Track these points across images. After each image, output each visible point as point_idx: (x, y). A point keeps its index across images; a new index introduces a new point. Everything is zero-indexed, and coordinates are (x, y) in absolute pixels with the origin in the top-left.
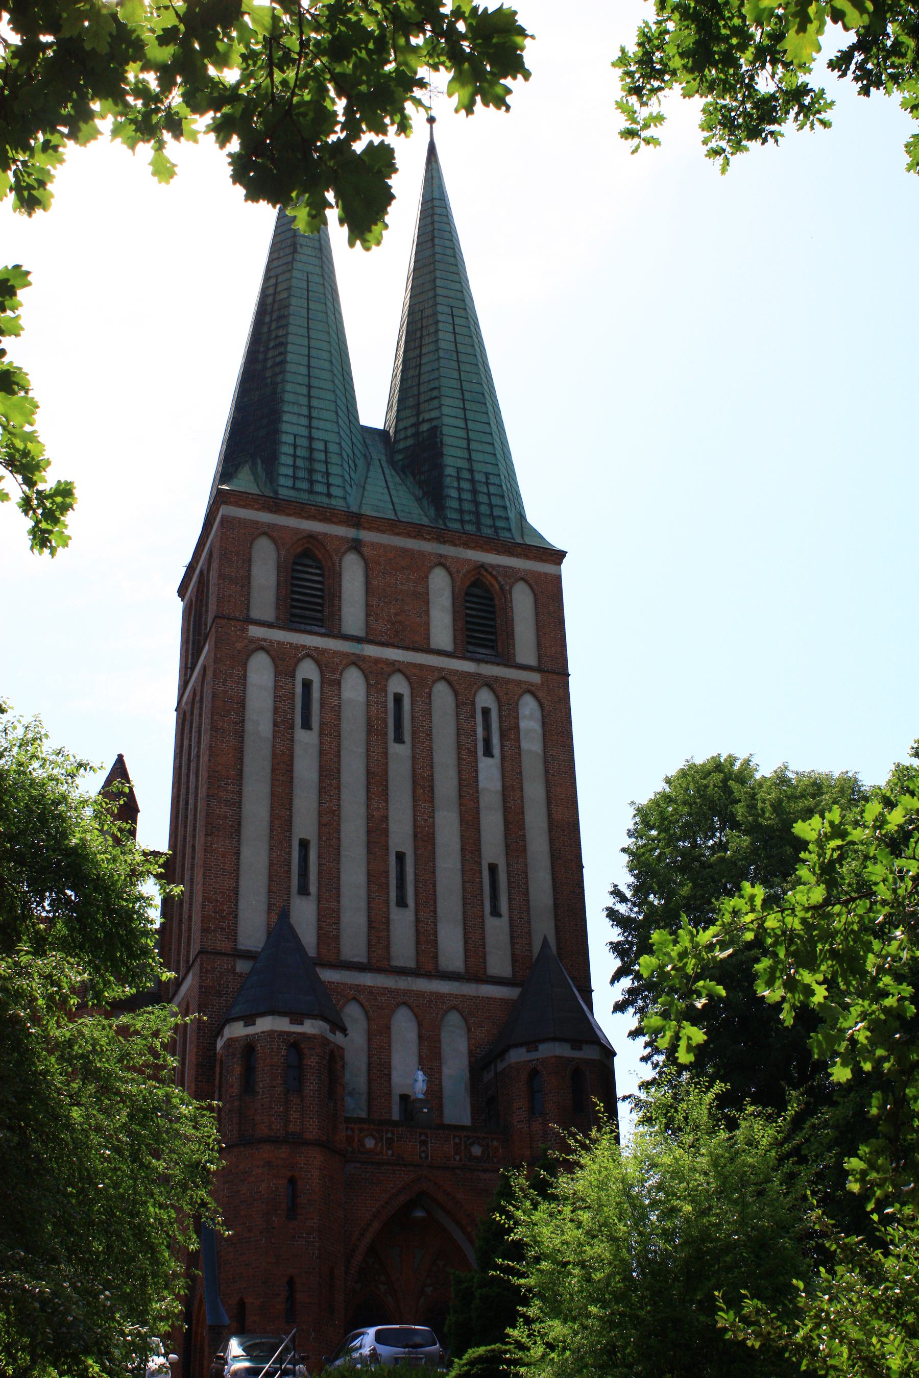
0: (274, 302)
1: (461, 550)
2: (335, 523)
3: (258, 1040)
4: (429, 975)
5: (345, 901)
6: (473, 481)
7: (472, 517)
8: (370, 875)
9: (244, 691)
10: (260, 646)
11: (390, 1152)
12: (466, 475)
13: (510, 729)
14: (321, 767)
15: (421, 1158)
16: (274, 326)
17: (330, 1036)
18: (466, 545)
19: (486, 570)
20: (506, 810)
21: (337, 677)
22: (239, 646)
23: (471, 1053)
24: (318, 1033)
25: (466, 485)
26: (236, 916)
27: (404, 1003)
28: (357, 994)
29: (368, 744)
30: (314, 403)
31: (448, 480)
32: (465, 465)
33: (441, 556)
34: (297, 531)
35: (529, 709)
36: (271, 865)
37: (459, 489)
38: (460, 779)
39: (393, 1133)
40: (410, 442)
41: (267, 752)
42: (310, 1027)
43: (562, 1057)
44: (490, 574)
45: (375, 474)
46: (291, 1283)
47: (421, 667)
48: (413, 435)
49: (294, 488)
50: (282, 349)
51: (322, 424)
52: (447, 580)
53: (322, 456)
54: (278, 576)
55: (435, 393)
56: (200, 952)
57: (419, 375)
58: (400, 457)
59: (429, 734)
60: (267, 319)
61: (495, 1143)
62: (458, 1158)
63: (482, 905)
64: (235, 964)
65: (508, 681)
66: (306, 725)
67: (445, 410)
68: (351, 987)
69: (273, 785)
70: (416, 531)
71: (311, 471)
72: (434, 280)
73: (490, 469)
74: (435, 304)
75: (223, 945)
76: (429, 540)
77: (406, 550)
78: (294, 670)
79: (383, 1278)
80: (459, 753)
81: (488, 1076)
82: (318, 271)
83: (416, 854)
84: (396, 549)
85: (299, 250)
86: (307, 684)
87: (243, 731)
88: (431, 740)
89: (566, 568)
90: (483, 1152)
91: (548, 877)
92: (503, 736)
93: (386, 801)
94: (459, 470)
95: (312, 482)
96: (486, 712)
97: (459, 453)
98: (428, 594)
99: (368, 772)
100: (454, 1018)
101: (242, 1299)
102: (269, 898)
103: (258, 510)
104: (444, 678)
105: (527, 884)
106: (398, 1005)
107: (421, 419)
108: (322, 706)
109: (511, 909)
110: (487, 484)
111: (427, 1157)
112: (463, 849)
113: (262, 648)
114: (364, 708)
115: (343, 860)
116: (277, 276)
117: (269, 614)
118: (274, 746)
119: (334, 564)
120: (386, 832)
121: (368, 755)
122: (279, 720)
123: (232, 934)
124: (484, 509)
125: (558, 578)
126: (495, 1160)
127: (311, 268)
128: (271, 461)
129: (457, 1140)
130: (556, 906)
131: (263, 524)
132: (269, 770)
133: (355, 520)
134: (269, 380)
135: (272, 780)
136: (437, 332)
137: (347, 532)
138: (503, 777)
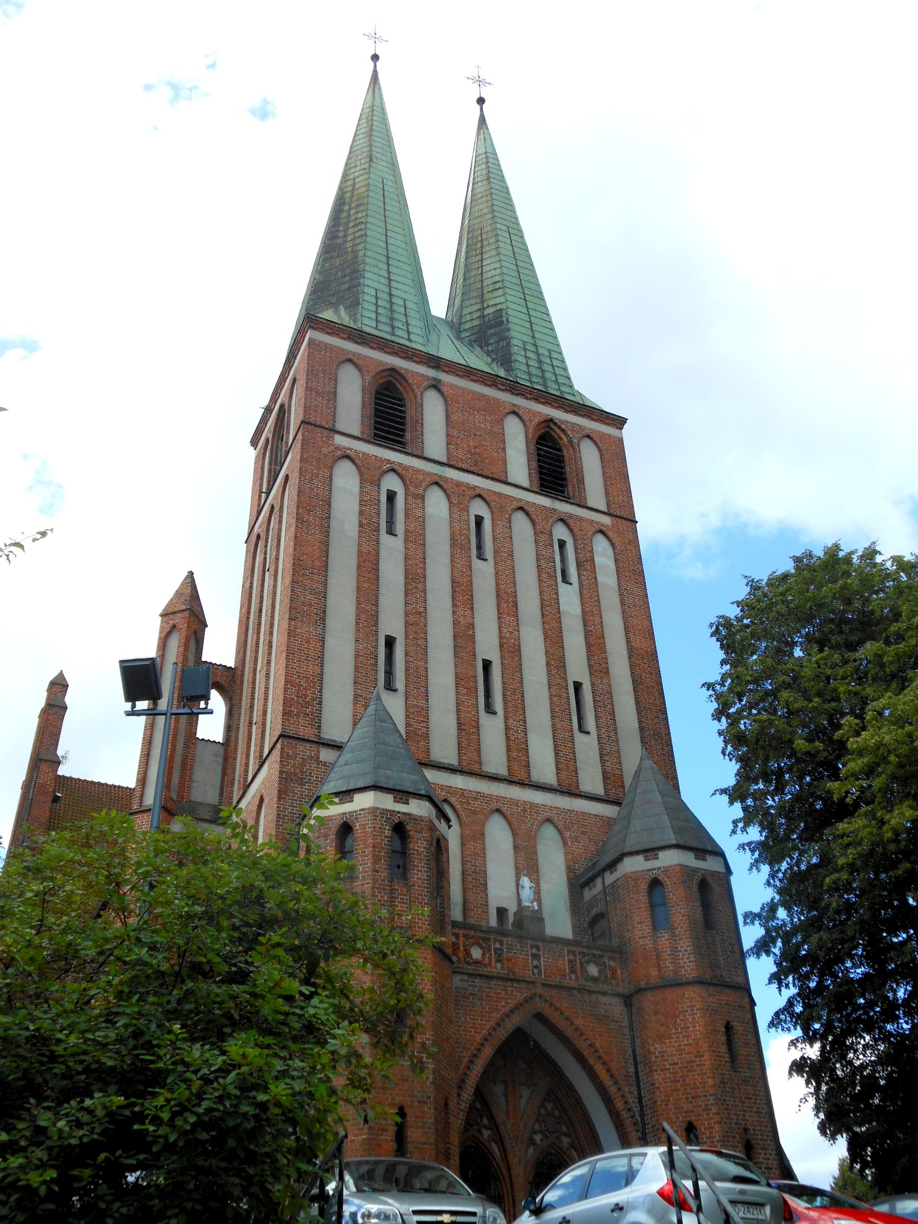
0: (352, 196)
3: (356, 819)
4: (521, 784)
8: (458, 679)
9: (330, 490)
12: (530, 347)
13: (586, 561)
15: (533, 973)
17: (436, 822)
19: (555, 424)
20: (587, 634)
21: (421, 492)
22: (325, 450)
23: (569, 869)
24: (426, 815)
26: (320, 703)
27: (498, 811)
29: (452, 556)
31: (515, 349)
32: (530, 340)
33: (514, 405)
34: (381, 363)
36: (357, 656)
37: (526, 357)
39: (502, 944)
41: (353, 550)
42: (418, 808)
43: (687, 866)
44: (559, 427)
47: (500, 495)
49: (376, 328)
50: (363, 226)
51: (400, 286)
56: (281, 736)
57: (482, 273)
59: (511, 555)
62: (573, 977)
63: (570, 719)
64: (318, 752)
65: (581, 519)
66: (391, 532)
69: (358, 581)
70: (492, 381)
73: (551, 347)
75: (307, 732)
76: (503, 390)
77: (483, 395)
78: (379, 480)
79: (485, 1121)
80: (540, 576)
81: (588, 894)
82: (392, 178)
83: (502, 664)
85: (374, 160)
88: (513, 560)
89: (627, 433)
90: (600, 972)
92: (579, 565)
93: (472, 609)
94: (524, 343)
95: (393, 327)
98: (504, 435)
99: (453, 581)
100: (549, 832)
102: (355, 690)
105: (612, 704)
107: (485, 305)
109: (598, 727)
110: (551, 358)
111: (540, 974)
112: (548, 664)
113: (348, 457)
114: (447, 523)
116: (354, 179)
118: (359, 545)
119: (415, 396)
120: (472, 638)
122: (365, 521)
123: (316, 721)
125: (621, 441)
128: (354, 306)
130: (641, 729)
131: (349, 352)
134: (350, 250)
135: (359, 575)
137: (431, 373)
138: (583, 603)
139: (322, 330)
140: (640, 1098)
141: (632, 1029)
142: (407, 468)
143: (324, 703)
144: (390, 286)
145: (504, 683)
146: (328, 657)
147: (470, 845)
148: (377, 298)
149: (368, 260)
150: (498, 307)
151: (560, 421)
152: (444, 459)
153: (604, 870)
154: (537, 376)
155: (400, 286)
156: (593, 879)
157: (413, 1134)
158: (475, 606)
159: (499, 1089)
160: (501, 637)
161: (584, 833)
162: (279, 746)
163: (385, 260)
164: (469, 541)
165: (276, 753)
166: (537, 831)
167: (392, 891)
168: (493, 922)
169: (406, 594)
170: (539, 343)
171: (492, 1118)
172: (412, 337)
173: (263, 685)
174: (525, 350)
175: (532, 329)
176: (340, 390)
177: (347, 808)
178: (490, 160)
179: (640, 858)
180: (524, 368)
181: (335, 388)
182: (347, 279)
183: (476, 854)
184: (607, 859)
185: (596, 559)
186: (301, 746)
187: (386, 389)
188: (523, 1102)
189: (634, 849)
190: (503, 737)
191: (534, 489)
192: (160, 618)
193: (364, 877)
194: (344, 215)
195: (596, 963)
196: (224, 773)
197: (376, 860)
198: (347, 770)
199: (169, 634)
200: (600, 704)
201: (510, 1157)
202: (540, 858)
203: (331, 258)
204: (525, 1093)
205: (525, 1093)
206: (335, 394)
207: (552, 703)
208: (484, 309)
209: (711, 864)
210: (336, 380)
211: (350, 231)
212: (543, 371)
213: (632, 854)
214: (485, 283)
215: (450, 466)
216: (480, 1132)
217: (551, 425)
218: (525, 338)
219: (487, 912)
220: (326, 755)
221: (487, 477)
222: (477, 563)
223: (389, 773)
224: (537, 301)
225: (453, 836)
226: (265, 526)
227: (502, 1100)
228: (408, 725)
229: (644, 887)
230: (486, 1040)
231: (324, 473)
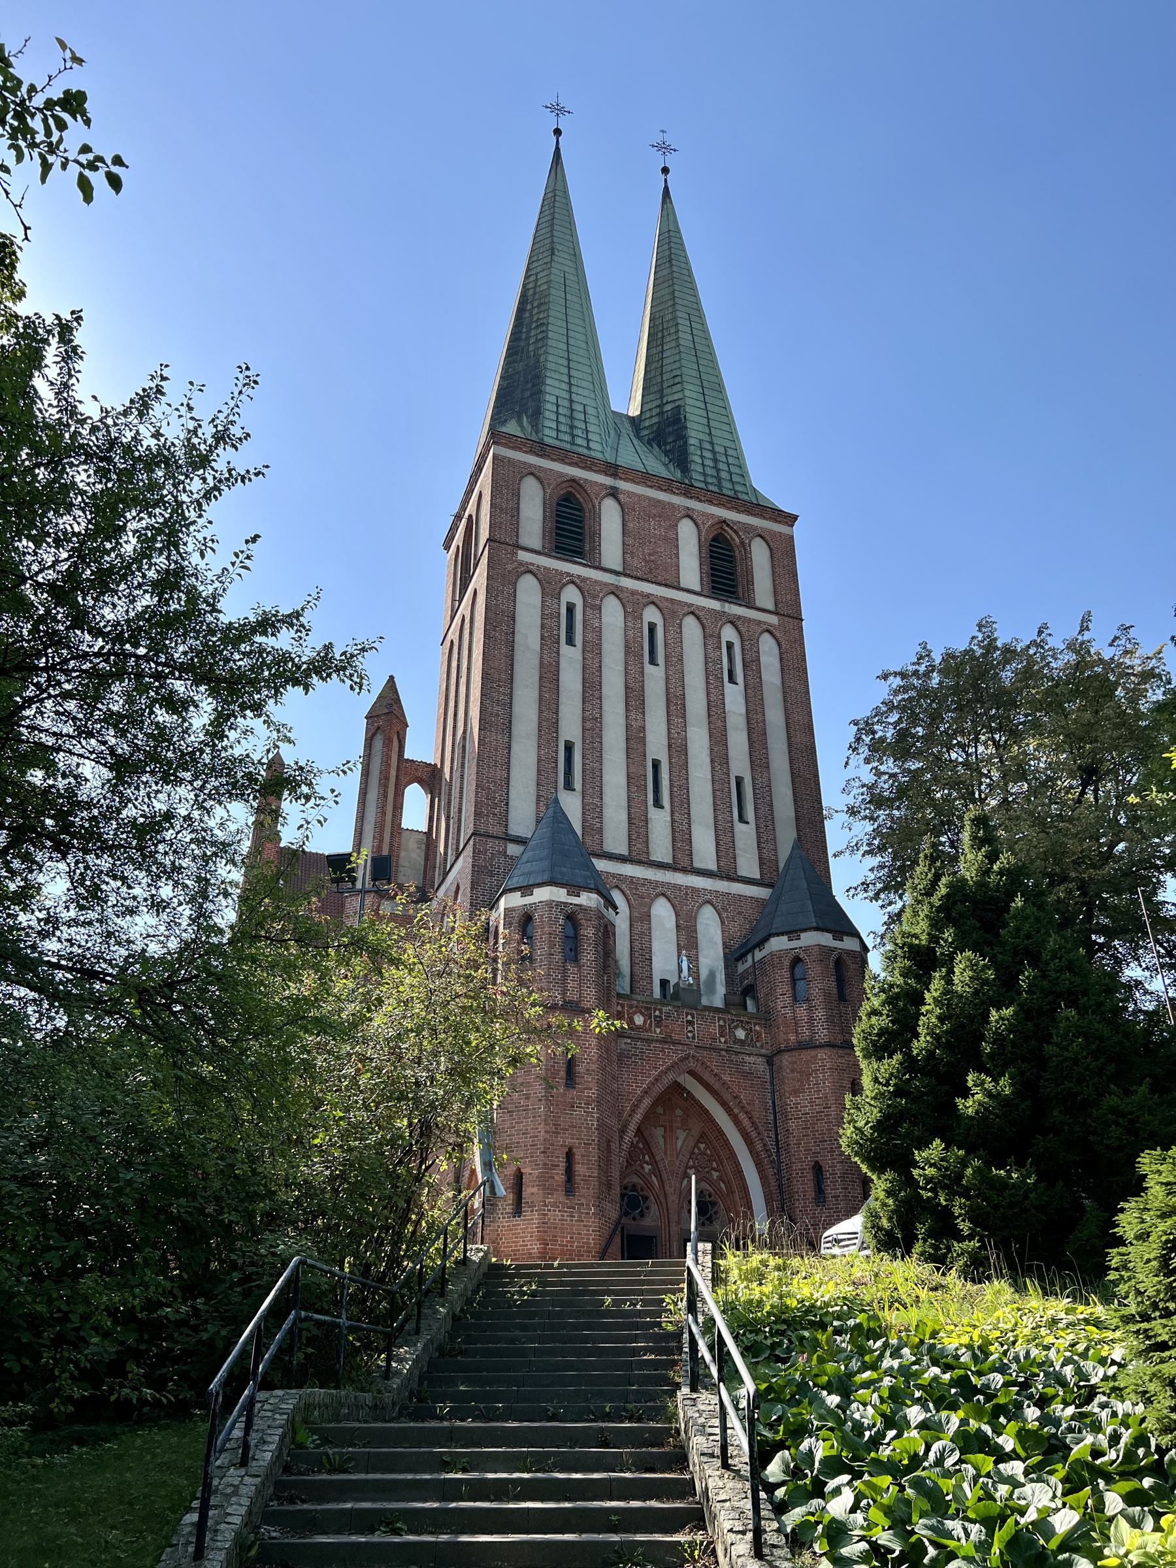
0: (535, 293)
1: (706, 505)
2: (595, 471)
4: (684, 870)
5: (607, 798)
6: (713, 452)
7: (714, 481)
11: (658, 1030)
14: (584, 679)
16: (535, 311)
17: (604, 911)
18: (711, 502)
19: (728, 525)
21: (598, 603)
22: (509, 567)
23: (725, 945)
25: (708, 455)
26: (507, 804)
27: (663, 895)
28: (621, 882)
30: (573, 373)
32: (707, 438)
34: (561, 475)
35: (768, 649)
36: (539, 761)
37: (702, 457)
38: (709, 702)
40: (655, 420)
42: (588, 899)
44: (732, 528)
45: (625, 441)
46: (569, 1155)
47: (672, 601)
48: (658, 414)
49: (557, 438)
50: (544, 328)
51: (580, 391)
52: (694, 530)
53: (582, 416)
54: (544, 511)
55: (678, 379)
56: (473, 834)
58: (646, 432)
60: (529, 307)
61: (757, 1028)
62: (723, 1040)
65: (749, 620)
66: (570, 642)
67: (687, 393)
68: (614, 876)
70: (666, 485)
71: (572, 427)
72: (673, 292)
73: (728, 443)
74: (675, 311)
75: (496, 830)
77: (659, 501)
79: (647, 1158)
80: (707, 678)
81: (742, 967)
82: (573, 271)
83: (670, 763)
84: (650, 499)
86: (571, 609)
87: (513, 641)
89: (798, 530)
91: (790, 793)
92: (745, 666)
93: (643, 713)
94: (701, 441)
95: (573, 436)
96: (730, 646)
97: (701, 428)
99: (627, 687)
101: (519, 1169)
103: (526, 452)
104: (692, 613)
105: (771, 796)
106: (657, 896)
108: (585, 627)
110: (726, 455)
111: (693, 1037)
115: (605, 762)
116: (537, 274)
117: (537, 544)
119: (594, 506)
120: (643, 740)
121: (626, 673)
123: (504, 820)
124: (724, 475)
125: (791, 538)
126: (758, 1044)
127: (567, 269)
128: (536, 416)
129: (722, 1023)
131: (531, 465)
132: (537, 679)
133: (612, 470)
136: (677, 331)
137: (607, 481)
139: (506, 445)
140: (777, 1141)
141: (772, 1083)
142: (585, 580)
143: (511, 803)
145: (671, 780)
146: (514, 761)
147: (638, 927)
148: (558, 406)
149: (549, 365)
152: (619, 569)
153: (754, 947)
154: (712, 476)
155: (580, 391)
156: (744, 955)
157: (580, 1169)
158: (646, 709)
159: (659, 1132)
160: (669, 738)
161: (740, 913)
162: (471, 842)
163: (566, 363)
165: (470, 848)
166: (698, 911)
167: (565, 970)
169: (584, 703)
170: (715, 440)
171: (652, 1156)
172: (592, 445)
173: (458, 785)
174: (701, 448)
175: (709, 426)
176: (522, 505)
177: (528, 900)
178: (673, 239)
179: (785, 938)
181: (518, 503)
182: (530, 385)
183: (643, 933)
184: (756, 939)
185: (762, 659)
186: (490, 843)
187: (564, 500)
188: (680, 1143)
189: (779, 931)
190: (669, 829)
191: (705, 593)
193: (541, 961)
194: (527, 315)
195: (743, 1028)
196: (427, 859)
197: (552, 945)
198: (527, 868)
199: (374, 735)
201: (667, 1187)
202: (699, 936)
203: (514, 362)
204: (682, 1135)
205: (682, 1135)
206: (518, 509)
209: (849, 944)
210: (519, 495)
211: (533, 333)
212: (718, 470)
213: (778, 934)
214: (665, 378)
215: (626, 575)
216: (643, 1168)
218: (702, 436)
219: (651, 983)
220: (513, 849)
221: (660, 584)
222: (649, 669)
223: (564, 869)
224: (715, 394)
225: (621, 922)
226: (458, 633)
227: (661, 1141)
228: (584, 821)
229: (787, 963)
230: (646, 1092)
231: (508, 590)
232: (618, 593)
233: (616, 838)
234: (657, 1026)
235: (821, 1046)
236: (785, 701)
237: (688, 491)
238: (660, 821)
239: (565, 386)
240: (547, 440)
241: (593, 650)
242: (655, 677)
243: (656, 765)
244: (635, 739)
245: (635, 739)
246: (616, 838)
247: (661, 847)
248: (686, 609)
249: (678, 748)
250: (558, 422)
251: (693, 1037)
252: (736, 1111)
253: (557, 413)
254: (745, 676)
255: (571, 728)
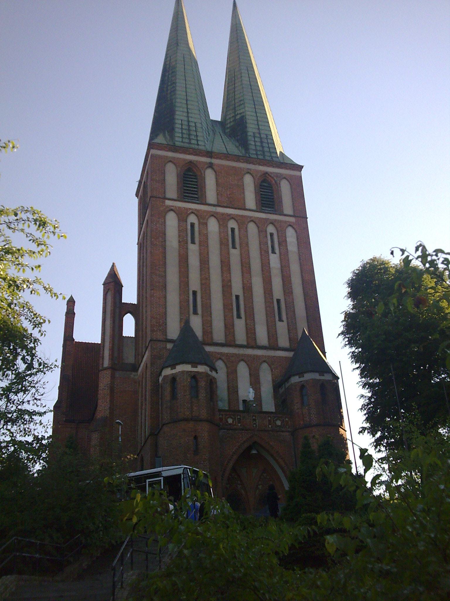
4: (252, 347)
5: (214, 316)
6: (261, 138)
9: (165, 228)
10: (171, 209)
12: (258, 135)
18: (260, 164)
19: (269, 175)
21: (206, 221)
22: (162, 209)
23: (273, 381)
24: (204, 371)
26: (166, 325)
28: (220, 357)
33: (248, 169)
34: (184, 160)
36: (180, 302)
37: (255, 141)
40: (232, 124)
42: (201, 369)
44: (271, 176)
47: (242, 216)
49: (182, 142)
55: (242, 102)
62: (270, 426)
63: (275, 317)
65: (281, 221)
66: (193, 242)
67: (246, 109)
68: (218, 353)
70: (237, 158)
73: (266, 132)
75: (160, 336)
79: (239, 482)
80: (261, 252)
81: (281, 391)
86: (192, 225)
92: (280, 244)
93: (230, 273)
95: (190, 139)
96: (272, 235)
105: (294, 307)
108: (199, 234)
111: (256, 427)
112: (265, 293)
113: (172, 210)
117: (174, 195)
119: (202, 174)
120: (230, 286)
122: (181, 240)
123: (164, 331)
124: (266, 149)
128: (172, 131)
142: (198, 211)
144: (188, 117)
150: (242, 115)
151: (271, 173)
152: (216, 203)
164: (228, 241)
168: (241, 408)
172: (200, 143)
180: (254, 148)
185: (287, 239)
191: (259, 210)
192: (103, 286)
195: (280, 420)
199: (107, 293)
200: (288, 308)
206: (164, 180)
207: (266, 311)
208: (236, 116)
209: (327, 377)
212: (263, 147)
213: (294, 375)
217: (267, 175)
218: (254, 131)
222: (232, 251)
232: (215, 215)
233: (219, 334)
234: (239, 423)
235: (314, 426)
236: (300, 259)
237: (248, 160)
238: (240, 326)
239: (185, 114)
240: (177, 144)
241: (204, 245)
242: (235, 254)
243: (237, 297)
244: (227, 286)
245: (227, 286)
246: (219, 334)
247: (241, 337)
248: (249, 219)
249: (248, 288)
250: (182, 133)
251: (256, 427)
252: (277, 458)
253: (182, 128)
254: (280, 249)
255: (195, 284)
